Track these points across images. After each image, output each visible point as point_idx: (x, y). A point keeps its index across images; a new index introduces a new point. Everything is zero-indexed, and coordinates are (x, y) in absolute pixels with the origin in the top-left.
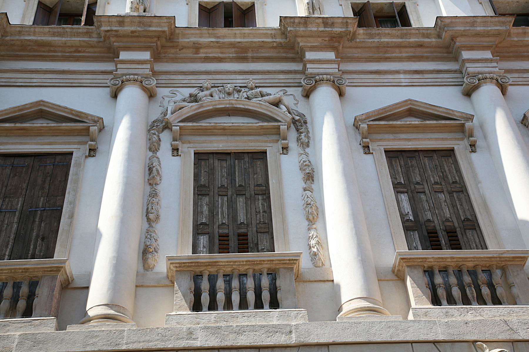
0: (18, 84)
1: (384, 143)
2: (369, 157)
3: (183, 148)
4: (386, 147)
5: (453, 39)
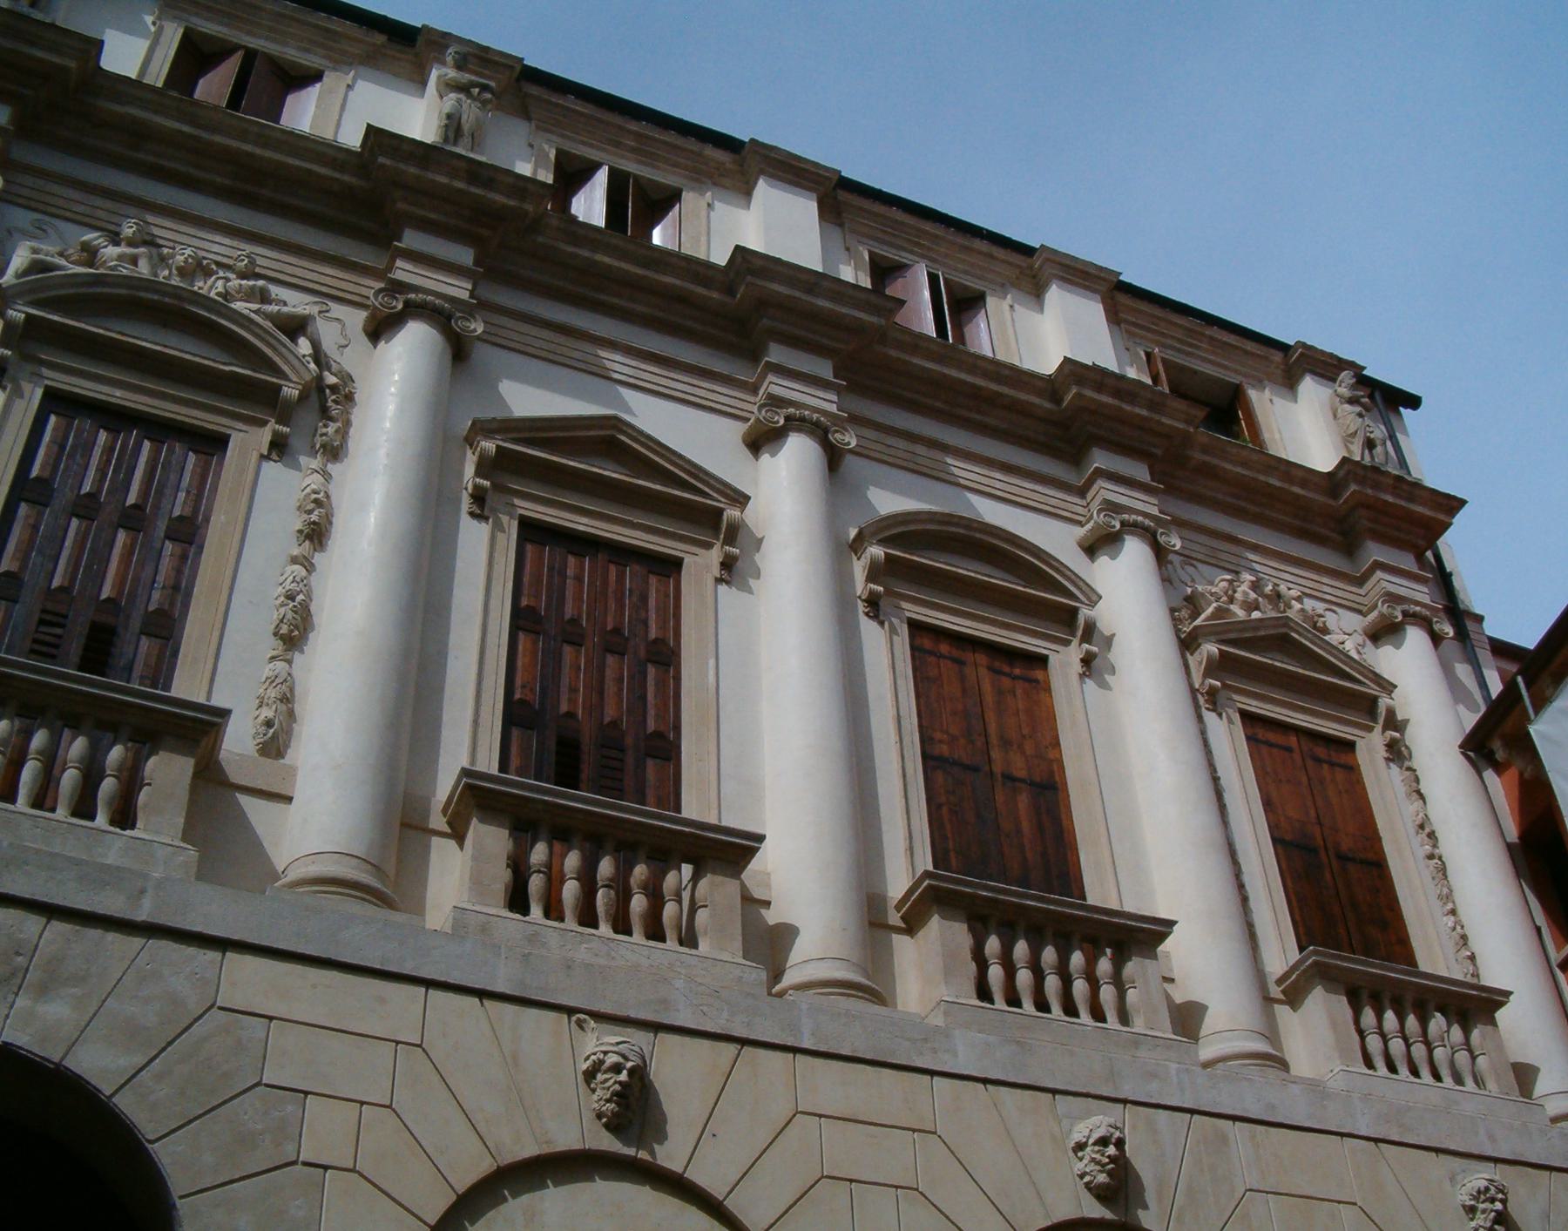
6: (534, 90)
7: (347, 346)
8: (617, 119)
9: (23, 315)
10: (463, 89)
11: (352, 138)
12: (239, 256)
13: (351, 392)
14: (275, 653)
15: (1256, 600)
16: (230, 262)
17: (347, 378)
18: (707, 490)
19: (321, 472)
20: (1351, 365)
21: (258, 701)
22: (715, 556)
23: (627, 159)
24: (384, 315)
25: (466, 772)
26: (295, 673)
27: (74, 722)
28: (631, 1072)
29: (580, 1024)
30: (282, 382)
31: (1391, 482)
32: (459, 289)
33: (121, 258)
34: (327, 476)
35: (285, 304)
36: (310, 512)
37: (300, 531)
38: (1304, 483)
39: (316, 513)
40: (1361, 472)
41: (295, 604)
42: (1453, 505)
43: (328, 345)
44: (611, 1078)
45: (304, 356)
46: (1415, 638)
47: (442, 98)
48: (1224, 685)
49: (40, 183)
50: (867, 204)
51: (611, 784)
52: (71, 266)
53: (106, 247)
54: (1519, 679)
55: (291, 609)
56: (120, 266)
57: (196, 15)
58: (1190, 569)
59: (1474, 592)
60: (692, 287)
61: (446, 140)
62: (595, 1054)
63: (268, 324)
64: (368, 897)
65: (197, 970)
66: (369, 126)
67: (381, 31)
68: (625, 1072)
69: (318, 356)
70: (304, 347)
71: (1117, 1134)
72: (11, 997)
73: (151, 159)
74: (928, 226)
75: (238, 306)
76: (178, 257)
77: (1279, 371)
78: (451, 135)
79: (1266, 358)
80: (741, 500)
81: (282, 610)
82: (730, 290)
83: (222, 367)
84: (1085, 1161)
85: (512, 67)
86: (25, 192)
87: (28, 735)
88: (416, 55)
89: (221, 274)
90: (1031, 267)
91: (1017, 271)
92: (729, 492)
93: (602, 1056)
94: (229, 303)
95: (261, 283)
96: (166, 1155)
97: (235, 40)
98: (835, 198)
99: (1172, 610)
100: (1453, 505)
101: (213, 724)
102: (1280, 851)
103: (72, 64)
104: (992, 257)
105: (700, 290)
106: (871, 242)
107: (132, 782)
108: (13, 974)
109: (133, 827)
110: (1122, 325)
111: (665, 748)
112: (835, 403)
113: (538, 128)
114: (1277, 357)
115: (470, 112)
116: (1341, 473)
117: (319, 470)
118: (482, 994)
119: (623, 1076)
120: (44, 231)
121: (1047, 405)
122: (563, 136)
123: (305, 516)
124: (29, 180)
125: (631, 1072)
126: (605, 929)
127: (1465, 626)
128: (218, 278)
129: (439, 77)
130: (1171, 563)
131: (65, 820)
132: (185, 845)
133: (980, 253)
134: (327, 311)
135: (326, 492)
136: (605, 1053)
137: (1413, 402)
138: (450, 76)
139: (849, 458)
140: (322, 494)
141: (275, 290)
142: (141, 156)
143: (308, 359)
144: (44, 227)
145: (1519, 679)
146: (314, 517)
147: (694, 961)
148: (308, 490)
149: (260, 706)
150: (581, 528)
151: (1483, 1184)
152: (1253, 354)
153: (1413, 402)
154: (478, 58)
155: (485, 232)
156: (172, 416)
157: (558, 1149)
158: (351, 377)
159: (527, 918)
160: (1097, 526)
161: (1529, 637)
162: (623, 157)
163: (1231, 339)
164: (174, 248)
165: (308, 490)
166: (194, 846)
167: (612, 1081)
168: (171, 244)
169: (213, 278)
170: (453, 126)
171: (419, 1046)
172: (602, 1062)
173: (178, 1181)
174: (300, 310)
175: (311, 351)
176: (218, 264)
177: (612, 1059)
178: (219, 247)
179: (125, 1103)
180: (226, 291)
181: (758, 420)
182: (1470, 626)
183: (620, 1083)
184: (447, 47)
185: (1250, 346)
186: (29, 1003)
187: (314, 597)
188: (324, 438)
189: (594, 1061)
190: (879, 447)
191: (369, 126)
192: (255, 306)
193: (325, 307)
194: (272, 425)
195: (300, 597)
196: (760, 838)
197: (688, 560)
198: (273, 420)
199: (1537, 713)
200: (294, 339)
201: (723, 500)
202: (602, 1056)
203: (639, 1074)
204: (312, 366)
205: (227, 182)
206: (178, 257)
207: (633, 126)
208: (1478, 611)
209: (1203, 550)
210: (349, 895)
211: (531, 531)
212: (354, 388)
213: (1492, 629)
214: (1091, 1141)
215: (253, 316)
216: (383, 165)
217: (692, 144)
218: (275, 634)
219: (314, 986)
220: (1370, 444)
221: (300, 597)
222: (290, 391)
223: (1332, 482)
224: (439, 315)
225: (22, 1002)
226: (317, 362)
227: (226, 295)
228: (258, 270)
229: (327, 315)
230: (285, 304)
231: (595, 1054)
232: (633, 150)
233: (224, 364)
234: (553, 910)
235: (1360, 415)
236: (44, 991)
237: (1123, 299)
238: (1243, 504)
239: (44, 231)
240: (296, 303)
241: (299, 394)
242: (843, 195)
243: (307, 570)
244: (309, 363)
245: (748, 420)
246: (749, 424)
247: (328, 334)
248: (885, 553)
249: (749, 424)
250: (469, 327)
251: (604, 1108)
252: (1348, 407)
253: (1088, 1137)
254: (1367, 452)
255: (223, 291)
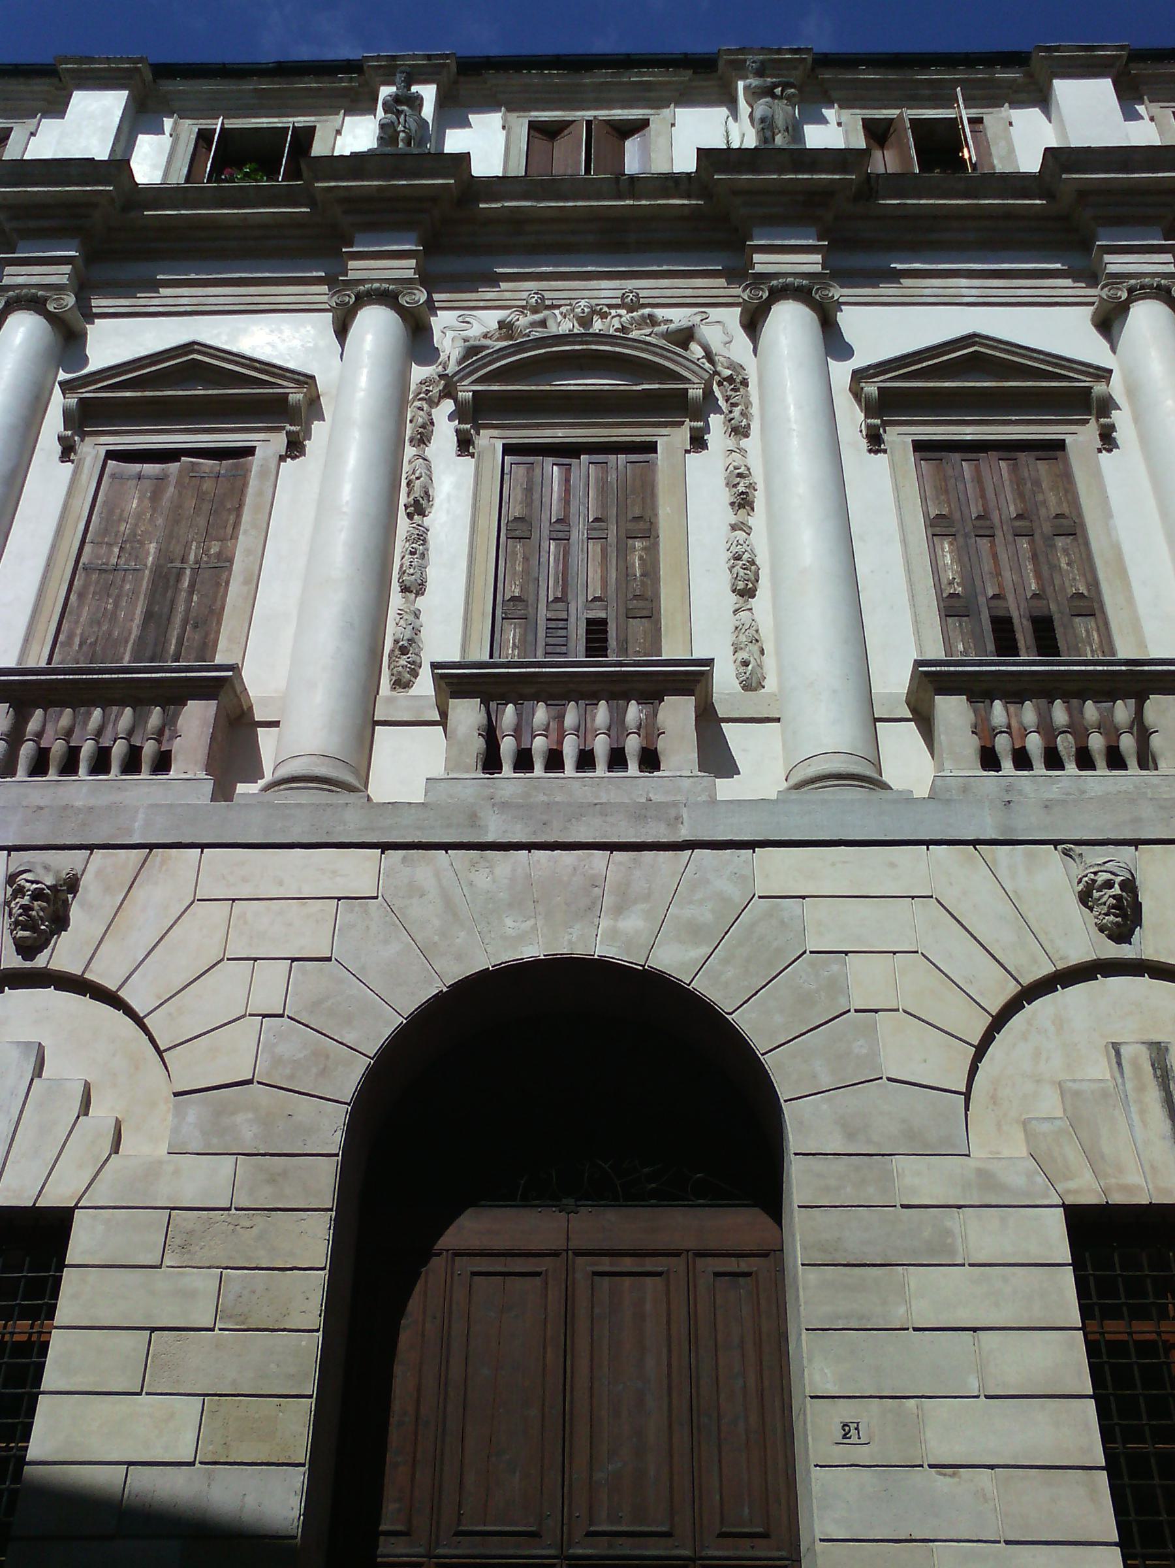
7: (731, 342)
9: (471, 394)
10: (769, 92)
11: (686, 163)
12: (624, 294)
13: (744, 379)
14: (737, 606)
18: (1071, 375)
19: (738, 451)
21: (732, 648)
24: (755, 306)
25: (918, 663)
26: (756, 617)
27: (593, 698)
28: (1122, 885)
29: (1066, 853)
30: (686, 386)
32: (812, 263)
33: (533, 324)
36: (735, 486)
37: (732, 504)
39: (741, 484)
41: (743, 562)
43: (716, 347)
44: (1105, 894)
48: (882, 421)
52: (496, 343)
53: (518, 320)
55: (742, 568)
56: (532, 331)
62: (1086, 876)
63: (663, 343)
64: (864, 784)
65: (735, 871)
66: (698, 149)
68: (1116, 886)
69: (709, 356)
70: (696, 350)
72: (596, 921)
75: (634, 334)
76: (576, 310)
80: (1105, 374)
87: (561, 718)
88: (720, 78)
89: (613, 312)
92: (1092, 370)
93: (1092, 876)
94: (628, 334)
95: (647, 311)
96: (745, 1021)
101: (702, 673)
107: (650, 730)
108: (594, 903)
109: (658, 768)
112: (1172, 263)
115: (782, 112)
117: (735, 450)
118: (975, 843)
119: (1116, 890)
120: (468, 322)
125: (1122, 885)
126: (1071, 768)
128: (613, 317)
129: (746, 88)
131: (604, 775)
132: (703, 774)
135: (745, 466)
136: (1095, 873)
138: (754, 85)
140: (743, 467)
141: (660, 313)
143: (704, 360)
144: (467, 319)
146: (741, 488)
147: (1155, 781)
149: (736, 652)
150: (968, 437)
156: (643, 439)
157: (1071, 964)
158: (741, 366)
159: (1000, 773)
164: (570, 305)
165: (731, 468)
166: (710, 773)
167: (1107, 896)
168: (568, 301)
169: (609, 318)
170: (766, 127)
172: (1094, 881)
173: (759, 1043)
174: (685, 323)
175: (703, 354)
176: (609, 306)
177: (1103, 877)
178: (607, 291)
179: (702, 986)
180: (622, 326)
183: (1114, 897)
186: (612, 922)
187: (756, 552)
188: (733, 422)
189: (1086, 882)
191: (698, 149)
192: (648, 331)
193: (704, 316)
194: (688, 423)
195: (746, 556)
197: (1069, 440)
198: (688, 420)
200: (686, 348)
201: (1088, 379)
202: (1092, 876)
203: (1130, 886)
204: (707, 365)
206: (576, 310)
210: (844, 785)
212: (746, 375)
215: (648, 339)
218: (734, 591)
219: (833, 864)
221: (746, 556)
222: (696, 392)
224: (801, 289)
225: (605, 923)
227: (623, 329)
228: (642, 301)
229: (707, 320)
231: (1086, 876)
234: (1022, 760)
236: (619, 910)
239: (468, 322)
240: (679, 317)
241: (703, 393)
243: (747, 533)
244: (703, 364)
245: (1092, 304)
246: (1095, 306)
247: (711, 335)
249: (1095, 306)
250: (828, 295)
251: (1105, 921)
255: (620, 327)
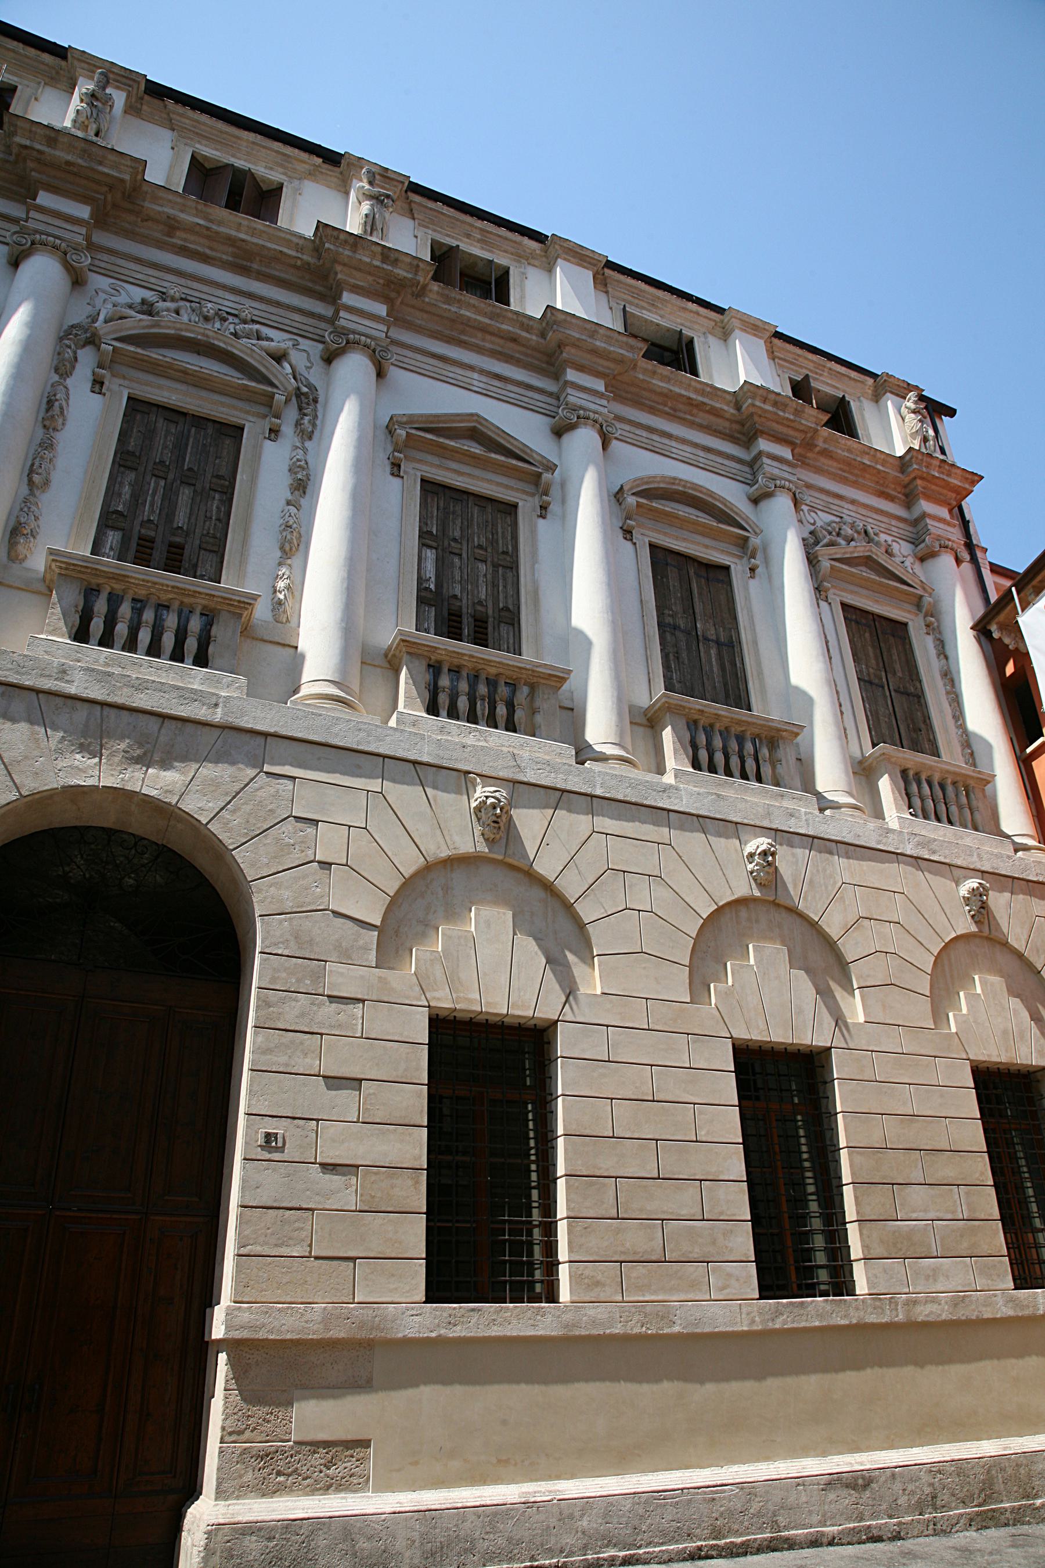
0: (629, 440)
1: (424, 468)
2: (397, 481)
3: (111, 383)
4: (424, 474)
5: (560, 346)
6: (417, 198)
8: (468, 219)
15: (852, 535)
16: (236, 312)
17: (312, 388)
20: (916, 388)
22: (536, 501)
23: (475, 247)
24: (334, 348)
31: (938, 463)
34: (305, 451)
35: (272, 340)
38: (884, 463)
40: (920, 457)
42: (975, 478)
45: (287, 374)
46: (947, 560)
47: (360, 203)
48: (832, 586)
49: (113, 259)
50: (622, 278)
51: (481, 639)
53: (158, 302)
54: (1013, 589)
57: (199, 142)
58: (813, 514)
59: (981, 535)
60: (519, 332)
61: (365, 231)
67: (318, 156)
71: (772, 849)
73: (180, 242)
74: (660, 293)
77: (870, 392)
78: (369, 229)
79: (862, 382)
81: (284, 534)
82: (543, 335)
83: (237, 381)
84: (754, 864)
85: (403, 183)
86: (103, 265)
88: (341, 173)
90: (722, 321)
91: (713, 323)
97: (225, 161)
98: (603, 274)
99: (804, 540)
100: (975, 478)
102: (863, 687)
103: (127, 177)
104: (698, 313)
105: (524, 334)
106: (750, 720)
110: (776, 360)
111: (511, 617)
113: (419, 224)
114: (870, 381)
116: (908, 457)
121: (732, 411)
122: (435, 231)
123: (294, 476)
124: (105, 257)
127: (976, 555)
130: (803, 510)
133: (691, 311)
134: (298, 345)
136: (487, 797)
137: (951, 412)
139: (614, 442)
141: (265, 331)
142: (174, 240)
145: (1013, 589)
148: (295, 459)
151: (976, 885)
152: (854, 379)
153: (951, 412)
154: (381, 175)
155: (393, 295)
160: (760, 488)
161: (1020, 567)
162: (471, 245)
163: (843, 370)
165: (295, 459)
171: (381, 793)
176: (228, 313)
181: (561, 418)
182: (979, 554)
184: (362, 168)
185: (853, 374)
190: (631, 435)
196: (569, 672)
199: (1023, 610)
204: (293, 380)
205: (230, 259)
207: (479, 224)
208: (983, 545)
209: (821, 503)
211: (429, 487)
213: (993, 557)
214: (758, 852)
216: (329, 249)
217: (516, 237)
219: (319, 759)
220: (925, 440)
223: (903, 463)
226: (295, 378)
230: (272, 340)
232: (479, 241)
233: (238, 379)
235: (920, 421)
237: (777, 342)
238: (846, 475)
242: (608, 272)
248: (637, 502)
252: (913, 415)
253: (756, 850)
254: (923, 444)
